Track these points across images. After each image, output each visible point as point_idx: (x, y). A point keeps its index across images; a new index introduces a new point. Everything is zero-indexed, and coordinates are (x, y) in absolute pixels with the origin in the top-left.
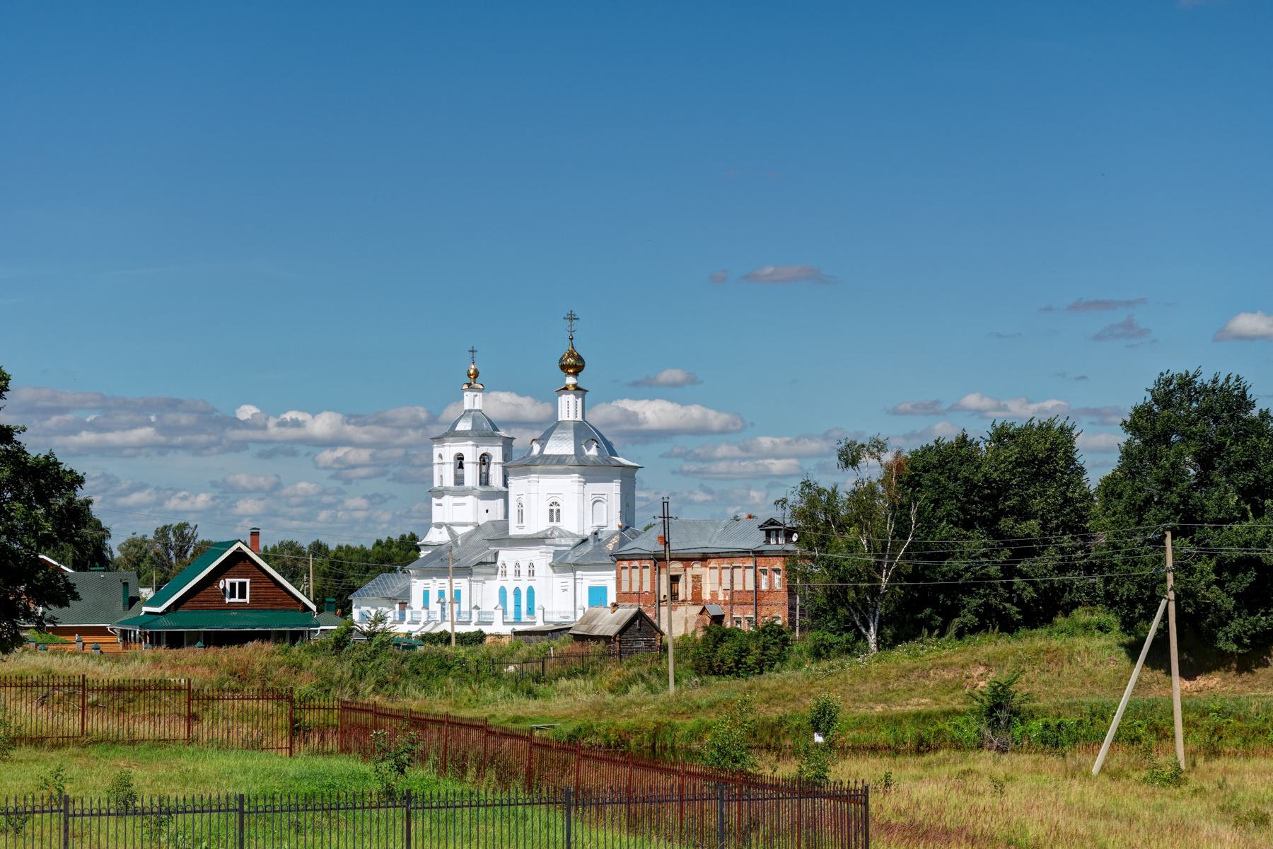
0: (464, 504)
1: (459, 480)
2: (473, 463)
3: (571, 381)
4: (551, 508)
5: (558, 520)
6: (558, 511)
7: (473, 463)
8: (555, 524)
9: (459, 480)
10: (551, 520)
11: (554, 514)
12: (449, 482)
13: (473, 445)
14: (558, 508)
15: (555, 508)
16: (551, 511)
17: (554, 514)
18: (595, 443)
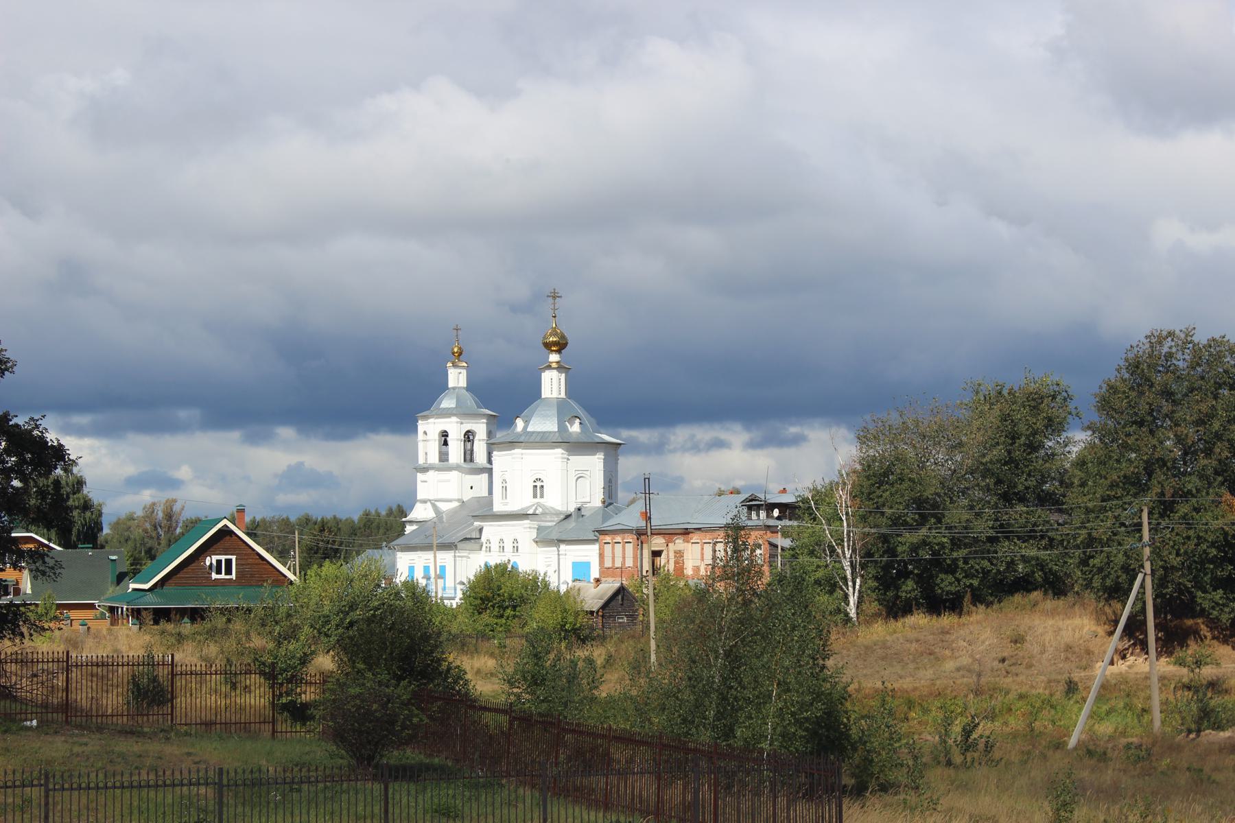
0: (448, 481)
1: (444, 457)
2: (458, 440)
3: (554, 358)
4: (535, 484)
5: (542, 496)
6: (542, 486)
7: (458, 440)
8: (538, 500)
9: (444, 457)
10: (535, 496)
11: (538, 489)
12: (434, 458)
13: (457, 423)
14: (542, 484)
15: (539, 484)
16: (536, 486)
17: (538, 489)
18: (578, 421)
